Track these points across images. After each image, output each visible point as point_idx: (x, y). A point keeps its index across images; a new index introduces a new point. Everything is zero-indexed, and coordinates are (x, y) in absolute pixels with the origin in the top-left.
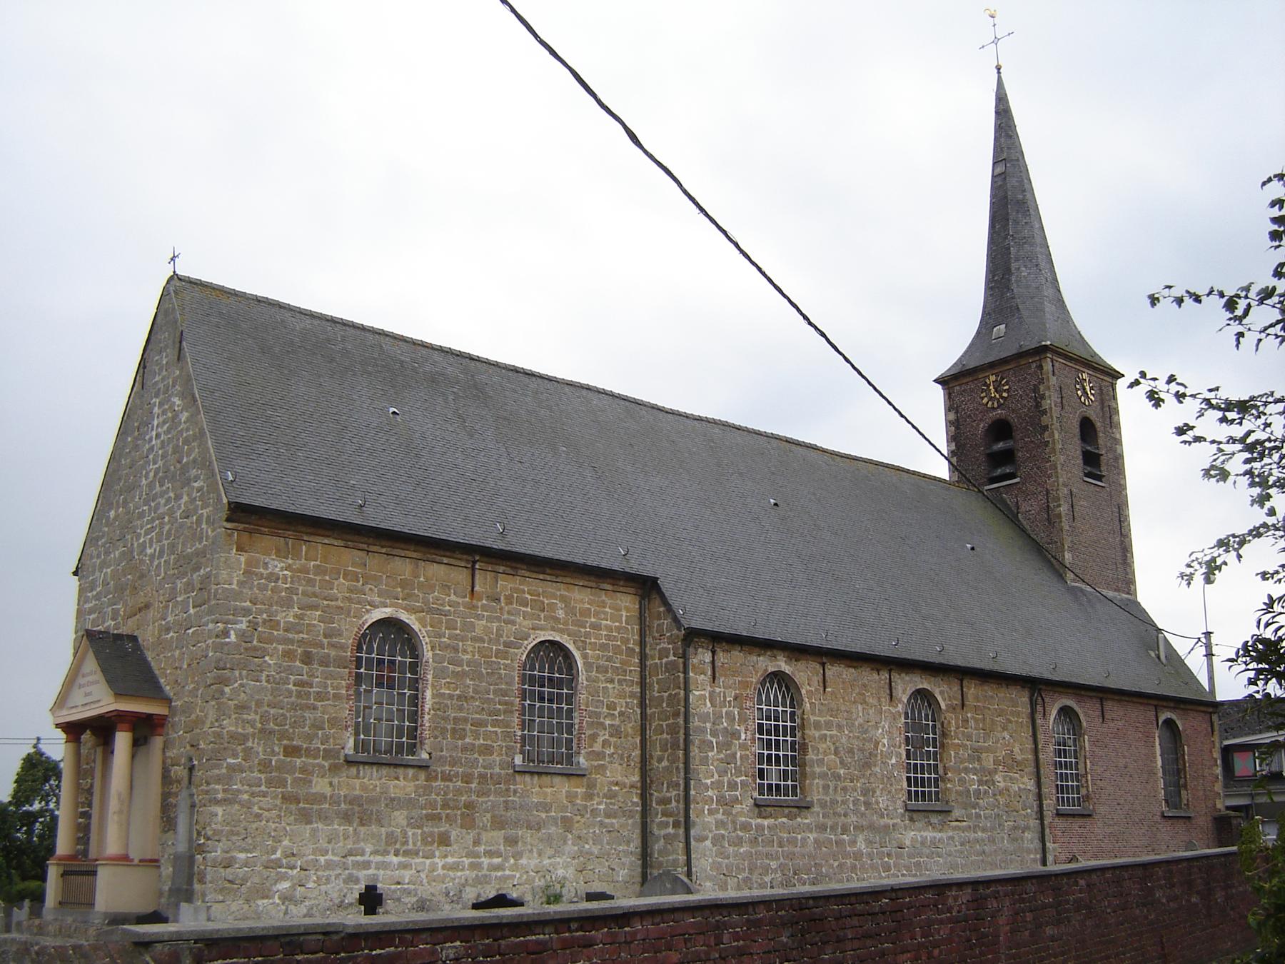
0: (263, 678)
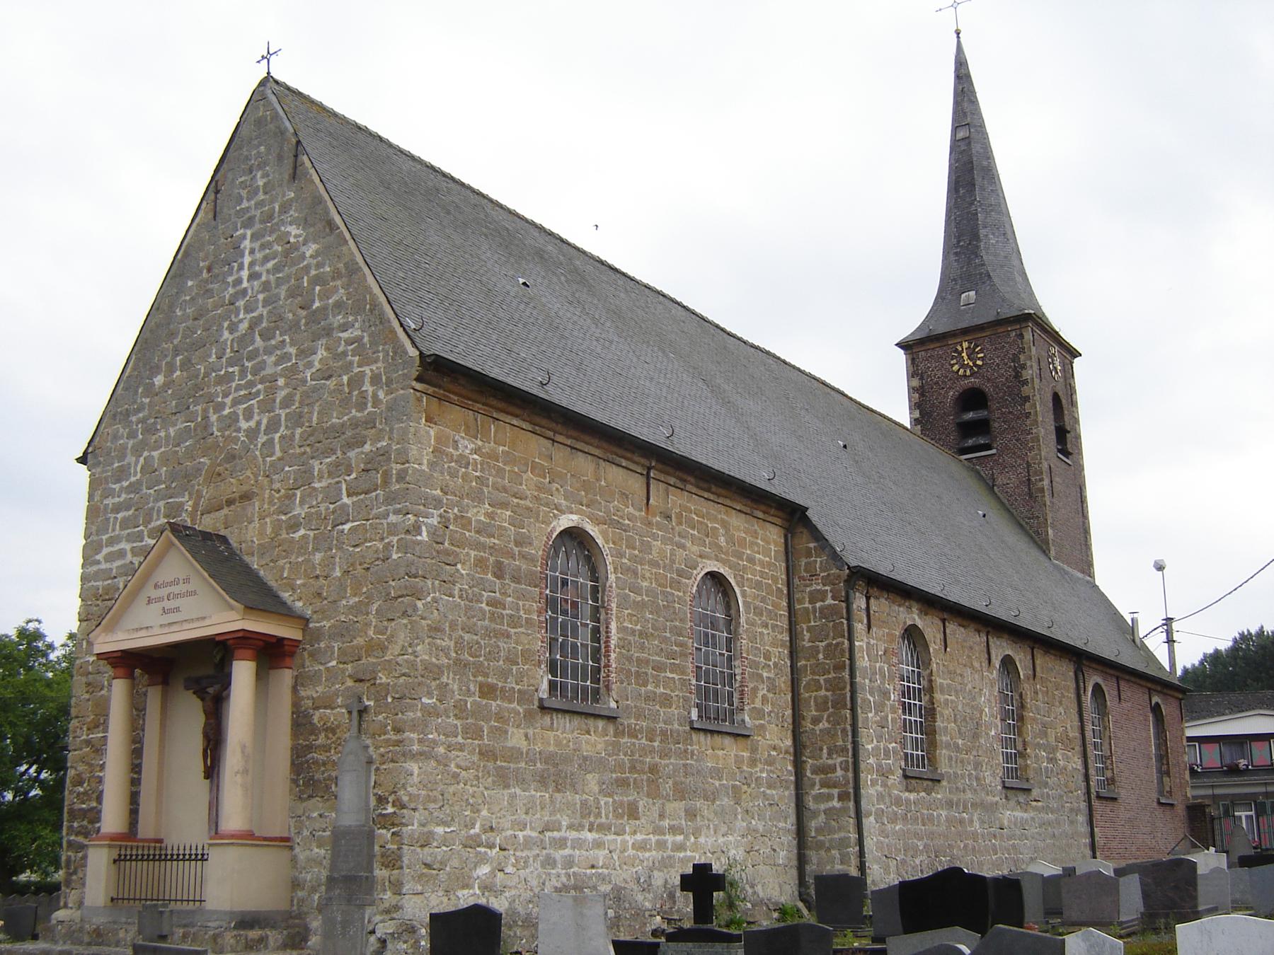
0: (456, 592)
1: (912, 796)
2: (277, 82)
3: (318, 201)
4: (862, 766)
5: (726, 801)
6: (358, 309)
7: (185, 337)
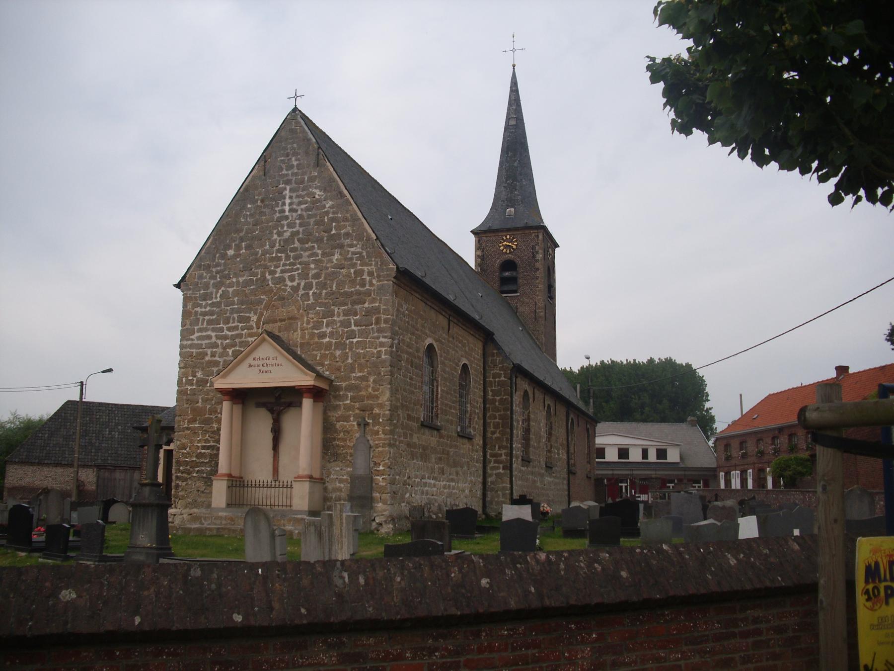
7: (247, 233)
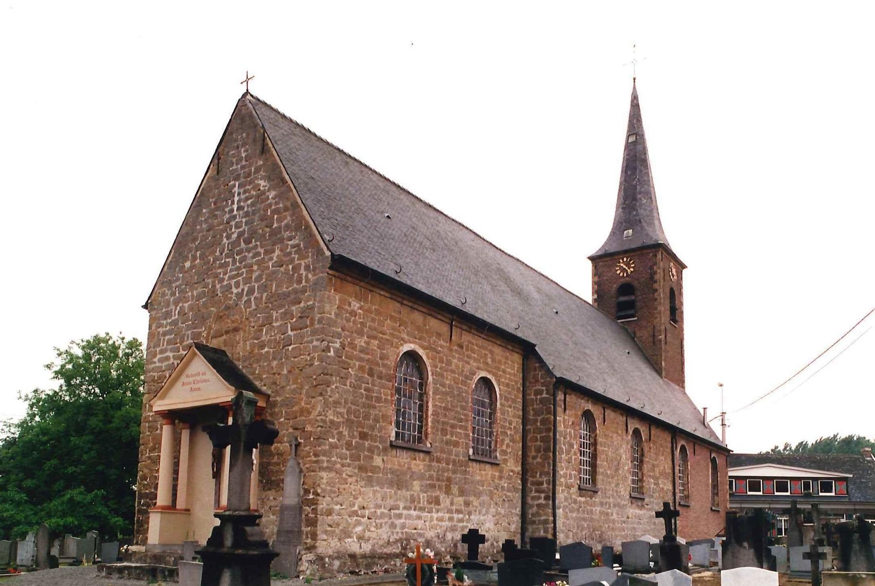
1: (583, 499)
2: (252, 96)
3: (275, 165)
4: (557, 483)
5: (485, 498)
6: (298, 228)
7: (201, 241)
